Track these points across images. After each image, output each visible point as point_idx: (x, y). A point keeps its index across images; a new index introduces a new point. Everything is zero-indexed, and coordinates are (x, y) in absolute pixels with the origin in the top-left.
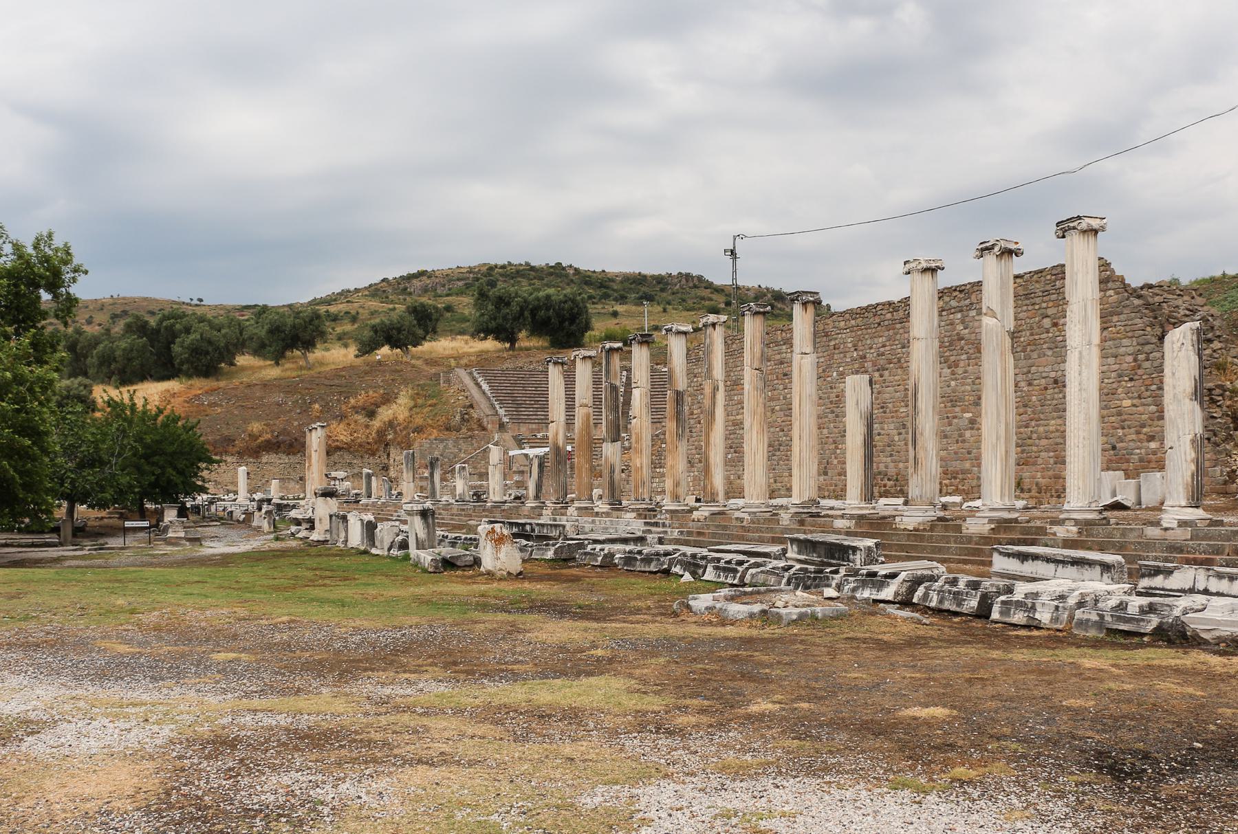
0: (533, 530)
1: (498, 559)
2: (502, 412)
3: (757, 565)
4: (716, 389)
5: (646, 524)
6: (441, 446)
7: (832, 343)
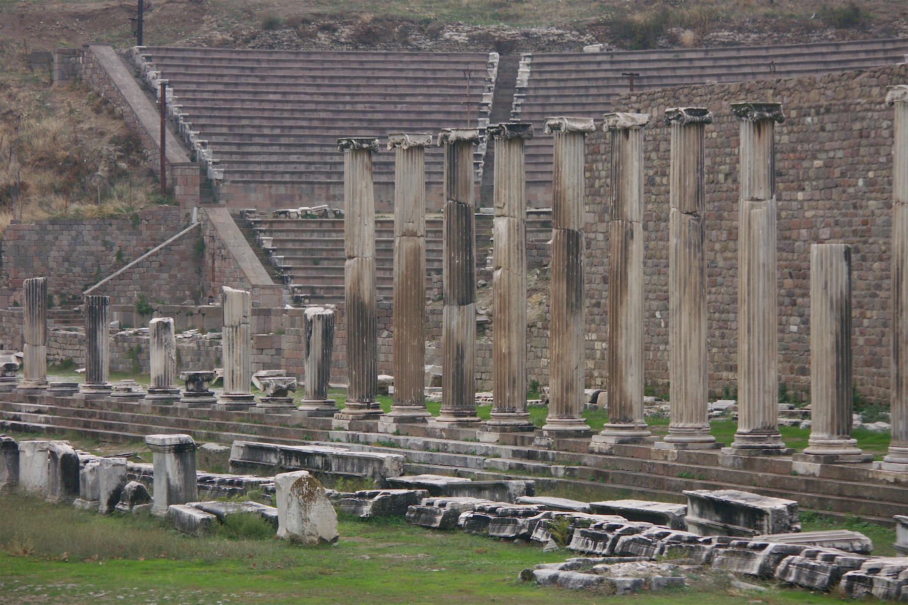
0: (327, 465)
1: (306, 520)
2: (206, 154)
3: (631, 531)
4: (628, 235)
5: (515, 454)
6: (65, 240)
7: (857, 126)
